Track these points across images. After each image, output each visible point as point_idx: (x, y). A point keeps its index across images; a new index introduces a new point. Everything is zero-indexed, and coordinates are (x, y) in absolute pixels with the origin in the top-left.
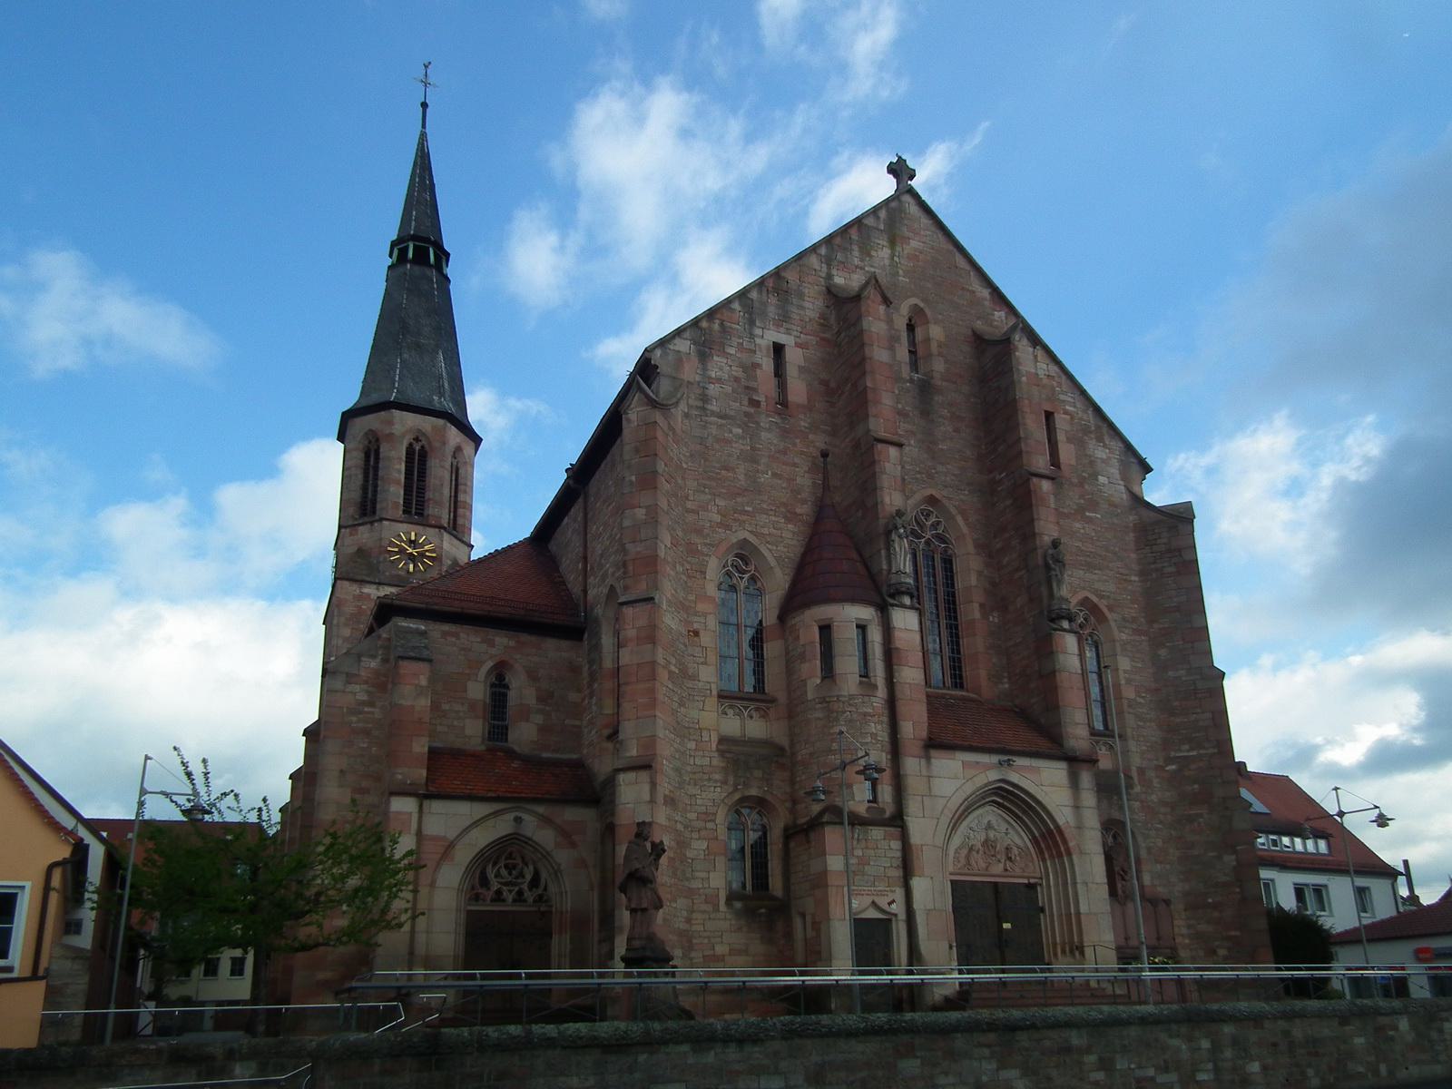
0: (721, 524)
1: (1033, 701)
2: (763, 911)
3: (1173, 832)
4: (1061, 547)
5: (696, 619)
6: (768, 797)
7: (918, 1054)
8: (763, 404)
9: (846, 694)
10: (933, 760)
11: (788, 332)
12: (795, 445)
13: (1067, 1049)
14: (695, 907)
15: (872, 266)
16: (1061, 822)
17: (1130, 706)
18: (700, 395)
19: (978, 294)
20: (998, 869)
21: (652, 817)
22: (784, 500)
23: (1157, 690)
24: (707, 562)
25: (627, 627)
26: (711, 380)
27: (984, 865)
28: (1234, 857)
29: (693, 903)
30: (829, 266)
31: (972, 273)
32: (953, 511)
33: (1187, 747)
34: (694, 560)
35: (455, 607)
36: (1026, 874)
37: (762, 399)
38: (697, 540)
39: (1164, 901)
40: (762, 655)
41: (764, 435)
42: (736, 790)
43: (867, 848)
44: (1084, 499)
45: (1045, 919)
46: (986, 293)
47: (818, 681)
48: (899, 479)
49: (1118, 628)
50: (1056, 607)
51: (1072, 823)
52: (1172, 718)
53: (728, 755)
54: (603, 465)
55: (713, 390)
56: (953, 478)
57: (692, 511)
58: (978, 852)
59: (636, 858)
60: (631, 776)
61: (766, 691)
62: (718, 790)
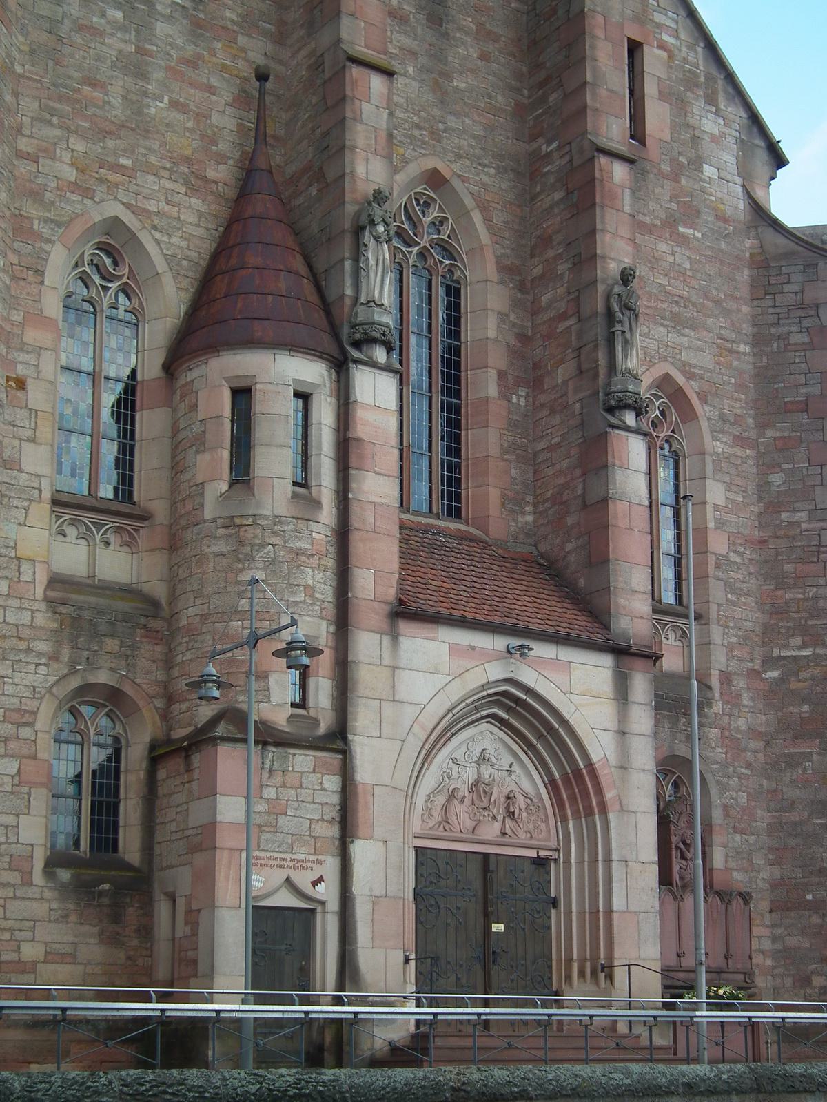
0: (75, 187)
1: (569, 547)
2: (106, 886)
3: (765, 782)
4: (635, 284)
5: (22, 357)
6: (128, 689)
9: (267, 513)
10: (402, 639)
12: (213, 52)
17: (718, 566)
22: (188, 152)
23: (763, 542)
24: (48, 253)
27: (468, 823)
32: (469, 202)
33: (798, 641)
39: (741, 894)
40: (133, 432)
41: (161, 28)
42: (73, 672)
43: (284, 785)
48: (384, 134)
49: (712, 431)
51: (613, 760)
52: (780, 592)
53: (63, 609)
61: (136, 499)
62: (43, 670)
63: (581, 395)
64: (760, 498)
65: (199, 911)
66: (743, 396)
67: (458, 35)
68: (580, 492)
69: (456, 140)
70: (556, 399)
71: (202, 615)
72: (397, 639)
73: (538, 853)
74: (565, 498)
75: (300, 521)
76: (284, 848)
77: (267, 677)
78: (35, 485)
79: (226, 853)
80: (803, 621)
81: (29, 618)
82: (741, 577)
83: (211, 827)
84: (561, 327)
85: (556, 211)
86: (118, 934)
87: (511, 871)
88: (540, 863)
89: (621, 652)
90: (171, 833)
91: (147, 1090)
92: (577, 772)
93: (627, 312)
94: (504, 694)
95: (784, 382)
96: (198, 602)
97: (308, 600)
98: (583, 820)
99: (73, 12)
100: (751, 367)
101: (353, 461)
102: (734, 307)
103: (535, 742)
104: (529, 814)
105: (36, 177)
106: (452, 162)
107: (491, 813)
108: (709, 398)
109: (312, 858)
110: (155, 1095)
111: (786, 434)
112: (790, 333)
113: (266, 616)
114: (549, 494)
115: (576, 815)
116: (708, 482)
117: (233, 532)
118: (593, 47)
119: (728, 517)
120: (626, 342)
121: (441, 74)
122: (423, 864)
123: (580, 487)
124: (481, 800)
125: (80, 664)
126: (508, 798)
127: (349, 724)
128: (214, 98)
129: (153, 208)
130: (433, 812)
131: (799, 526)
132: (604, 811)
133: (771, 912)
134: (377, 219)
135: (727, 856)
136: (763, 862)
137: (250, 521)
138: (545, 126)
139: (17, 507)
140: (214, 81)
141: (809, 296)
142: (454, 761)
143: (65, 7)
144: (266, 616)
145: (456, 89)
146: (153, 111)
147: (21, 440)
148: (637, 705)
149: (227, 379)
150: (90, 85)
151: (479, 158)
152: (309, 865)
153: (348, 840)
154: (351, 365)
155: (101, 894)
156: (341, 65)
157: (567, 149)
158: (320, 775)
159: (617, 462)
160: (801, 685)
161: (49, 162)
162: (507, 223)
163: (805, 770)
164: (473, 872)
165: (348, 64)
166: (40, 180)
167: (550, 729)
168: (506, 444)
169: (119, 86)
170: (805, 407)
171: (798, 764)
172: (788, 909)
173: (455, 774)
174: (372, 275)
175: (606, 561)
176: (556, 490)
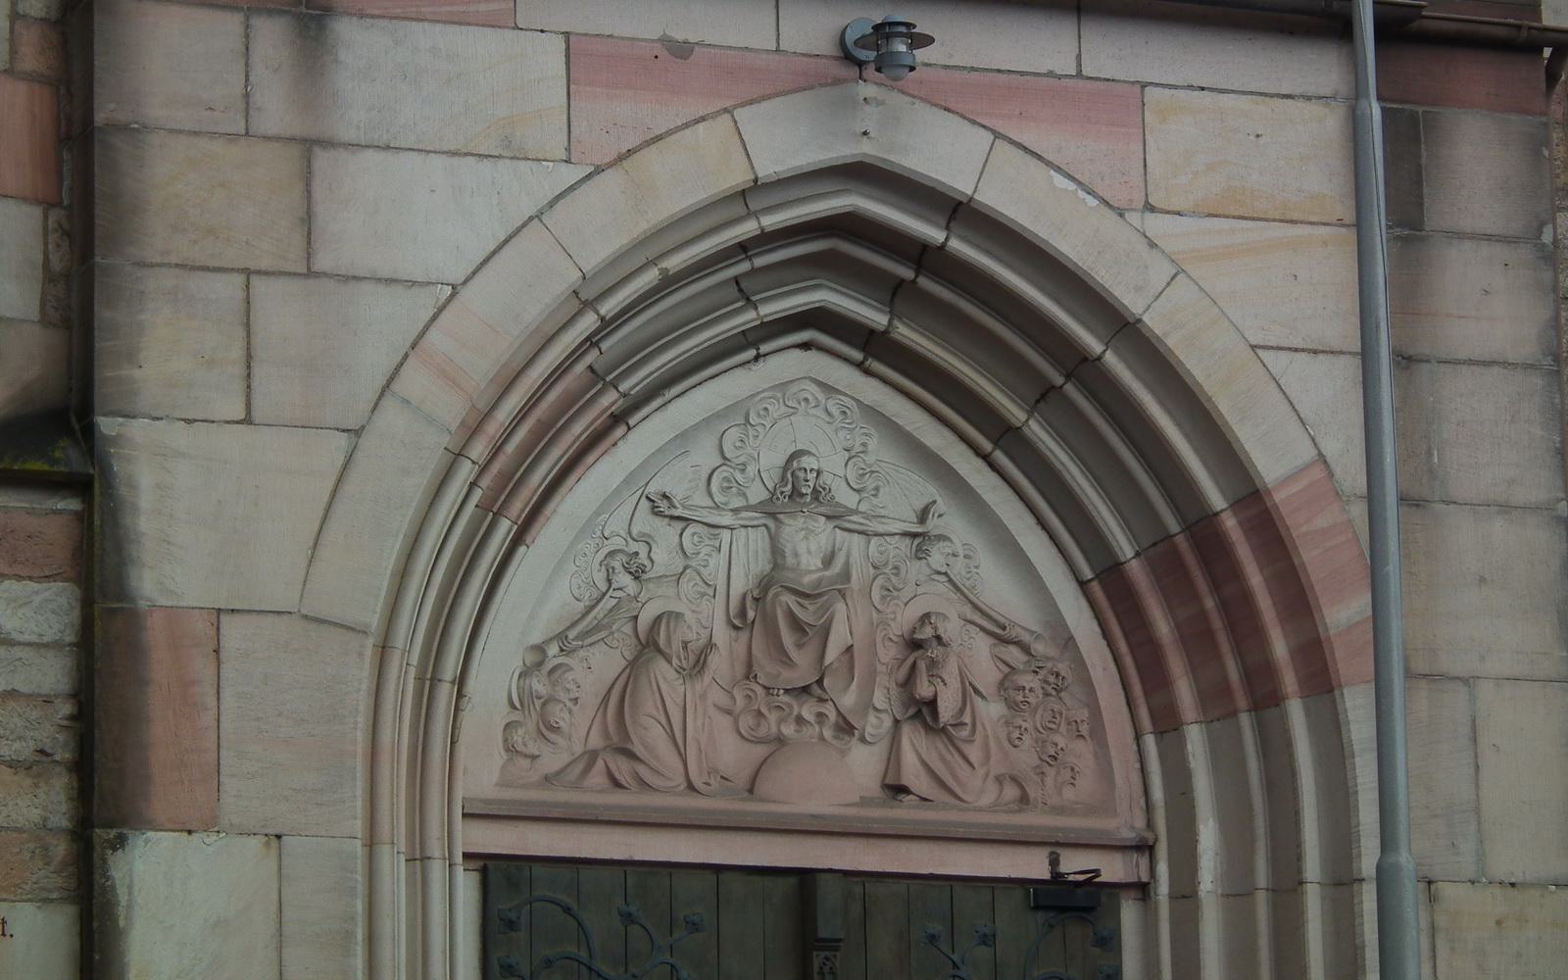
36: (1033, 819)
72: (322, 28)
73: (1054, 862)
87: (933, 939)
92: (1204, 529)
98: (1245, 720)
103: (1015, 413)
104: (1013, 706)
107: (829, 711)
115: (1216, 702)
122: (511, 925)
124: (786, 660)
127: (104, 373)
130: (559, 715)
132: (1321, 682)
142: (660, 506)
148: (1467, 245)
153: (100, 834)
167: (1080, 366)
173: (664, 557)
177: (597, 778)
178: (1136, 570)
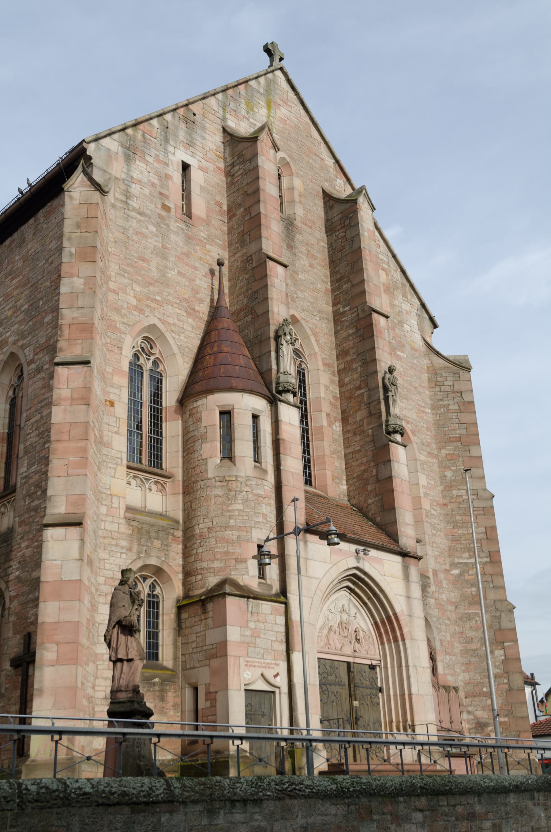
0: (136, 308)
1: (370, 501)
2: (157, 680)
3: (457, 628)
4: (395, 374)
5: (112, 390)
6: (165, 568)
7: (375, 817)
8: (173, 210)
9: (243, 475)
10: (309, 544)
11: (193, 155)
12: (195, 251)
13: (471, 816)
14: (99, 673)
15: (254, 120)
16: (398, 610)
17: (427, 516)
18: (124, 190)
19: (326, 162)
20: (348, 650)
21: (80, 576)
22: (186, 297)
23: (445, 505)
24: (124, 339)
25: (61, 386)
26: (132, 180)
27: (339, 646)
28: (502, 652)
29: (97, 669)
30: (224, 109)
31: (322, 144)
32: (309, 332)
33: (467, 555)
34: (114, 336)
35: (222, 287)
36: (369, 656)
37: (171, 205)
38: (115, 317)
39: (454, 688)
40: (161, 433)
41: (173, 237)
42: (139, 558)
43: (258, 621)
44: (396, 340)
45: (383, 696)
46: (331, 162)
47: (218, 461)
48: (284, 294)
49: (419, 449)
50: (393, 422)
51: (406, 612)
52: (456, 530)
53: (133, 523)
54: (7, 242)
55: (135, 189)
56: (309, 304)
57: (113, 291)
58: (335, 633)
59: (124, 606)
60: (60, 531)
61: (164, 467)
62: (124, 556)
63: (371, 426)
64: (442, 483)
65: (216, 692)
66: (430, 433)
67: (300, 255)
68: (374, 474)
69: (302, 303)
70: (356, 428)
71: (209, 528)
74: (365, 476)
75: (259, 480)
76: (260, 656)
77: (246, 561)
78: (119, 456)
79: (233, 658)
80: (468, 545)
81: (117, 527)
82: (437, 522)
83: (223, 645)
84: (358, 393)
85: (351, 338)
86: (163, 707)
88: (372, 667)
89: (404, 554)
90: (193, 648)
91: (287, 788)
93: (393, 387)
94: (354, 575)
95: (448, 427)
96: (205, 521)
97: (264, 521)
98: (393, 644)
99: (134, 225)
100: (431, 419)
101: (282, 450)
102: (422, 391)
104: (365, 640)
105: (118, 301)
106: (301, 313)
108: (416, 433)
109: (273, 662)
110: (291, 791)
111: (452, 452)
112: (449, 404)
113: (244, 529)
114: (355, 475)
116: (420, 474)
117: (225, 484)
118: (366, 264)
119: (429, 492)
120: (394, 401)
121: (294, 271)
123: (375, 471)
125: (142, 553)
126: (355, 631)
128: (197, 272)
129: (171, 322)
130: (322, 638)
131: (462, 498)
133: (466, 698)
134: (287, 333)
135: (444, 667)
136: (460, 671)
137: (234, 479)
138: (342, 299)
139: (110, 468)
140: (197, 264)
141: (457, 387)
143: (130, 223)
144: (244, 529)
145: (300, 279)
146: (170, 275)
147: (112, 432)
149: (218, 406)
150: (142, 260)
151: (312, 312)
152: (272, 666)
153: (290, 652)
154: (279, 403)
155: (154, 684)
156: (264, 260)
157: (355, 310)
158: (274, 616)
159: (394, 459)
160: (470, 577)
161: (124, 295)
162: (325, 343)
163: (476, 621)
164: (343, 671)
165: (267, 260)
166: (120, 303)
167: (375, 594)
168: (332, 450)
169: (155, 262)
170: (459, 439)
171: (473, 618)
172: (474, 697)
173: (330, 618)
174: (286, 359)
175: (394, 508)
176: (359, 473)
177: (327, 648)
178: (379, 623)
